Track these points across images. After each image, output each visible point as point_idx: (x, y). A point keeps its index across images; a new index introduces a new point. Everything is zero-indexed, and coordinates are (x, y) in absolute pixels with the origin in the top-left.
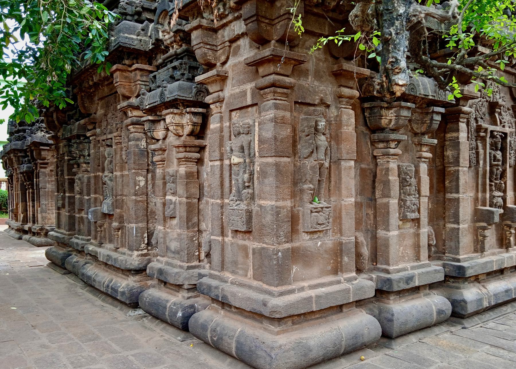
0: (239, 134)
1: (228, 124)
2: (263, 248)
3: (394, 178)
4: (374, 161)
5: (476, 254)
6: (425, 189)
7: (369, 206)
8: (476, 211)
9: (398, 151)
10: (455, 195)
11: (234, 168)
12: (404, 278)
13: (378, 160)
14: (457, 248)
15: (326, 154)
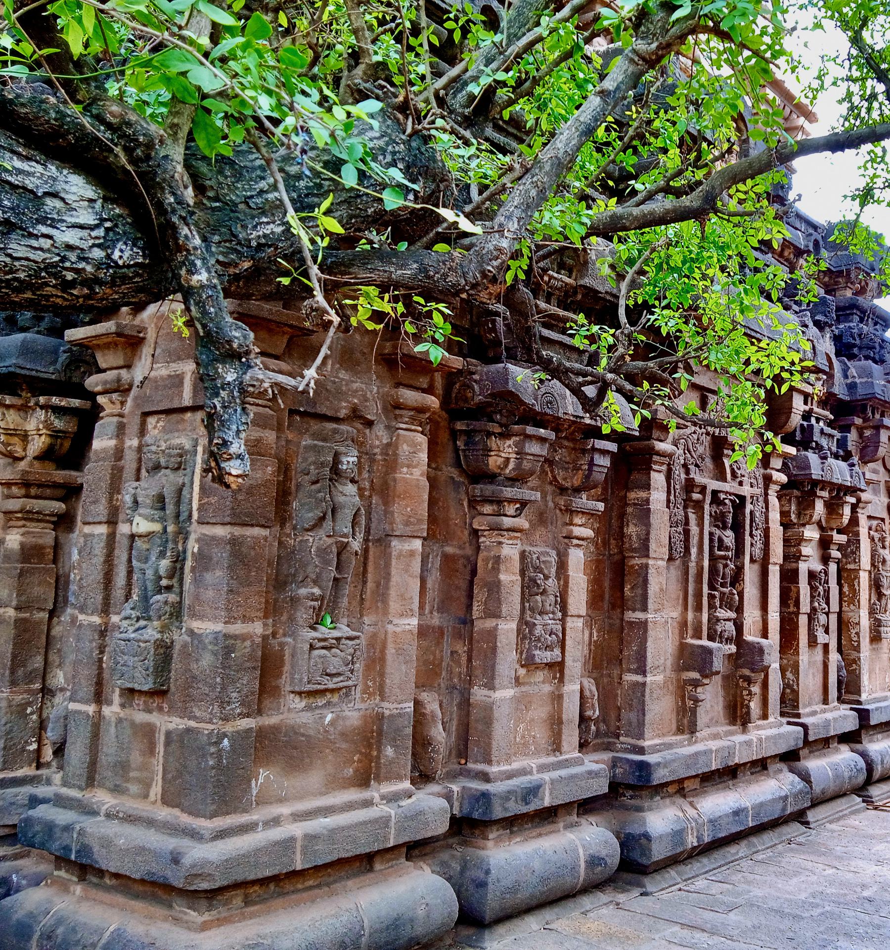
0: (157, 467)
1: (135, 442)
2: (188, 730)
3: (510, 578)
4: (474, 542)
5: (679, 738)
6: (578, 600)
7: (458, 635)
8: (683, 648)
9: (522, 522)
10: (640, 615)
11: (139, 543)
12: (519, 790)
13: (482, 539)
14: (641, 724)
15: (354, 523)
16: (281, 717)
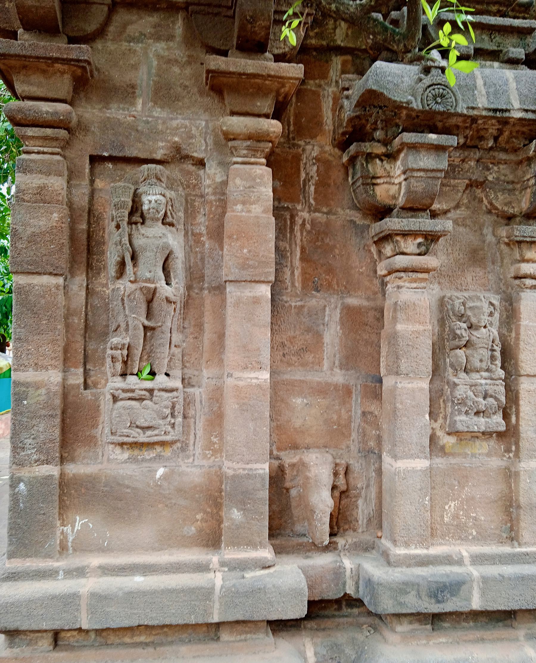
16: (100, 467)
